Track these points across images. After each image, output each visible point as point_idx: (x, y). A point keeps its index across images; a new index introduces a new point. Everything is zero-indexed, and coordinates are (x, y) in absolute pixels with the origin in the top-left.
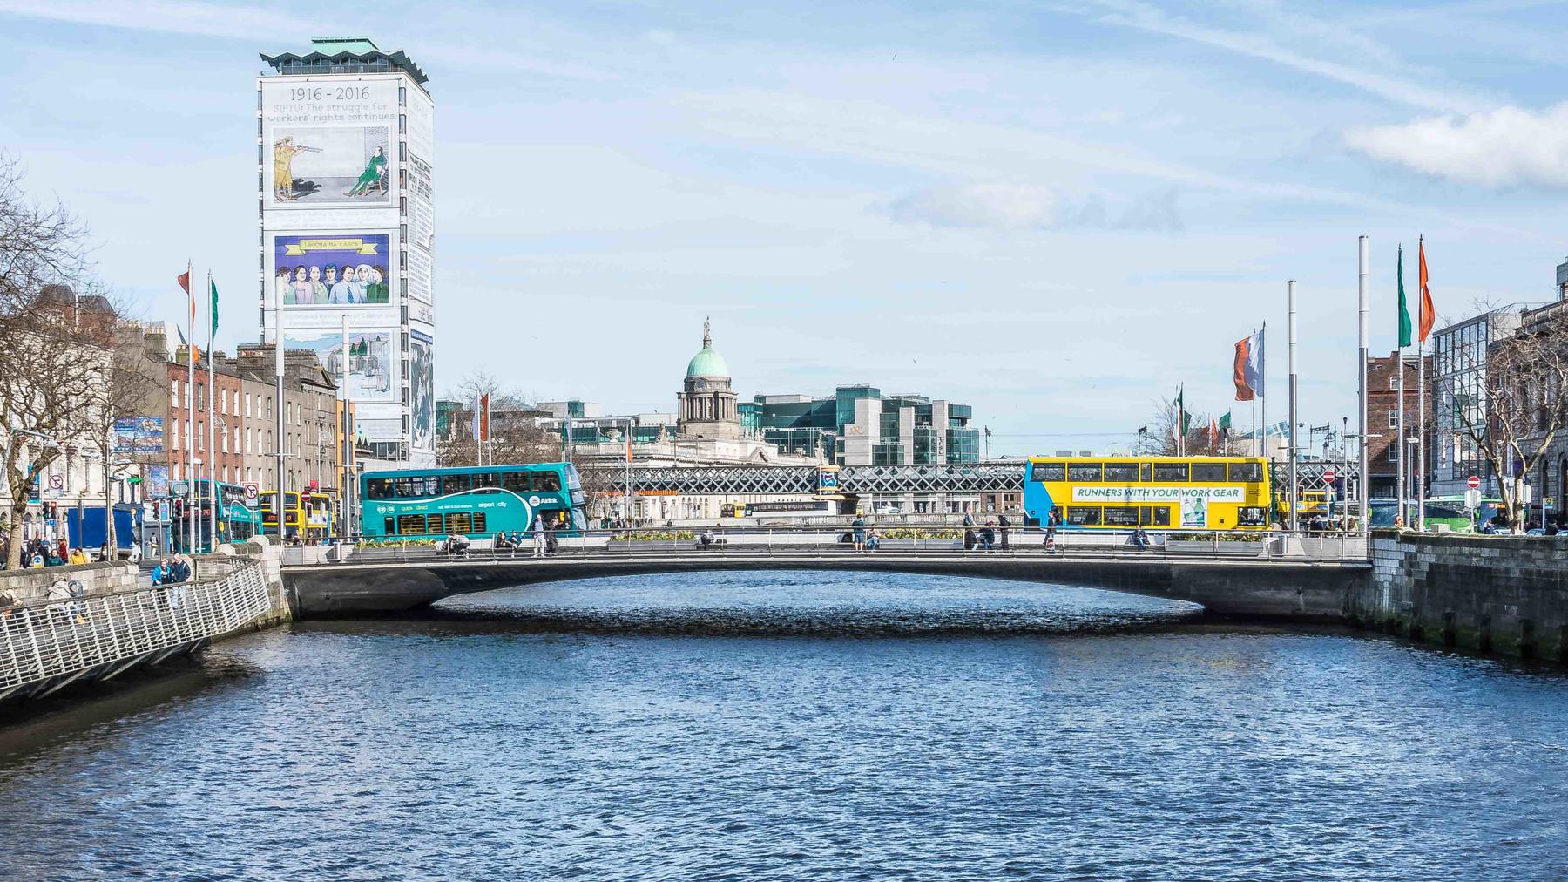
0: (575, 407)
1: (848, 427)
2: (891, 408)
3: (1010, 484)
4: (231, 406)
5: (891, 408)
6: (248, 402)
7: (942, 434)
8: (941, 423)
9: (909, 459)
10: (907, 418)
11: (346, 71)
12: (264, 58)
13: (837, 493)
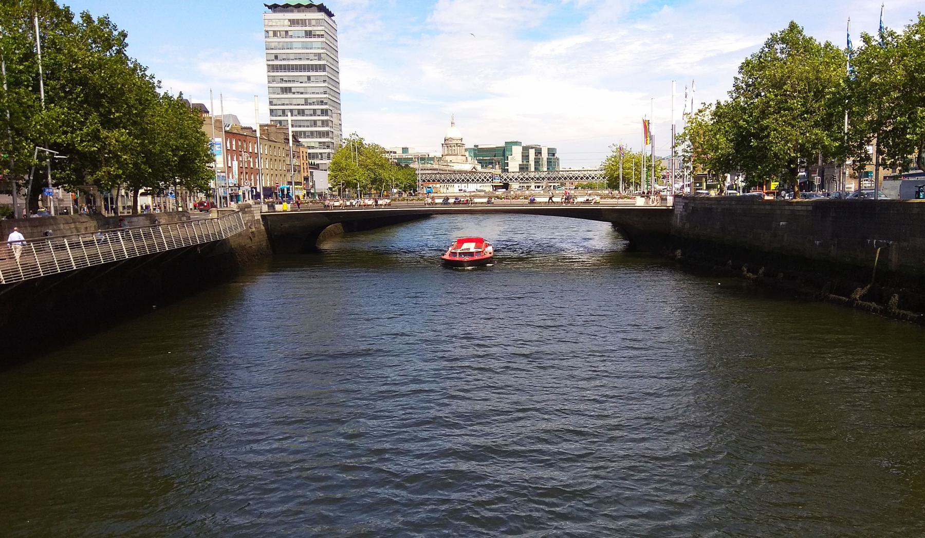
0: (405, 150)
1: (509, 157)
2: (526, 149)
3: (571, 178)
4: (253, 149)
5: (526, 149)
6: (234, 143)
7: (545, 159)
8: (545, 155)
9: (533, 169)
10: (532, 153)
11: (298, 12)
12: (266, 5)
13: (500, 182)
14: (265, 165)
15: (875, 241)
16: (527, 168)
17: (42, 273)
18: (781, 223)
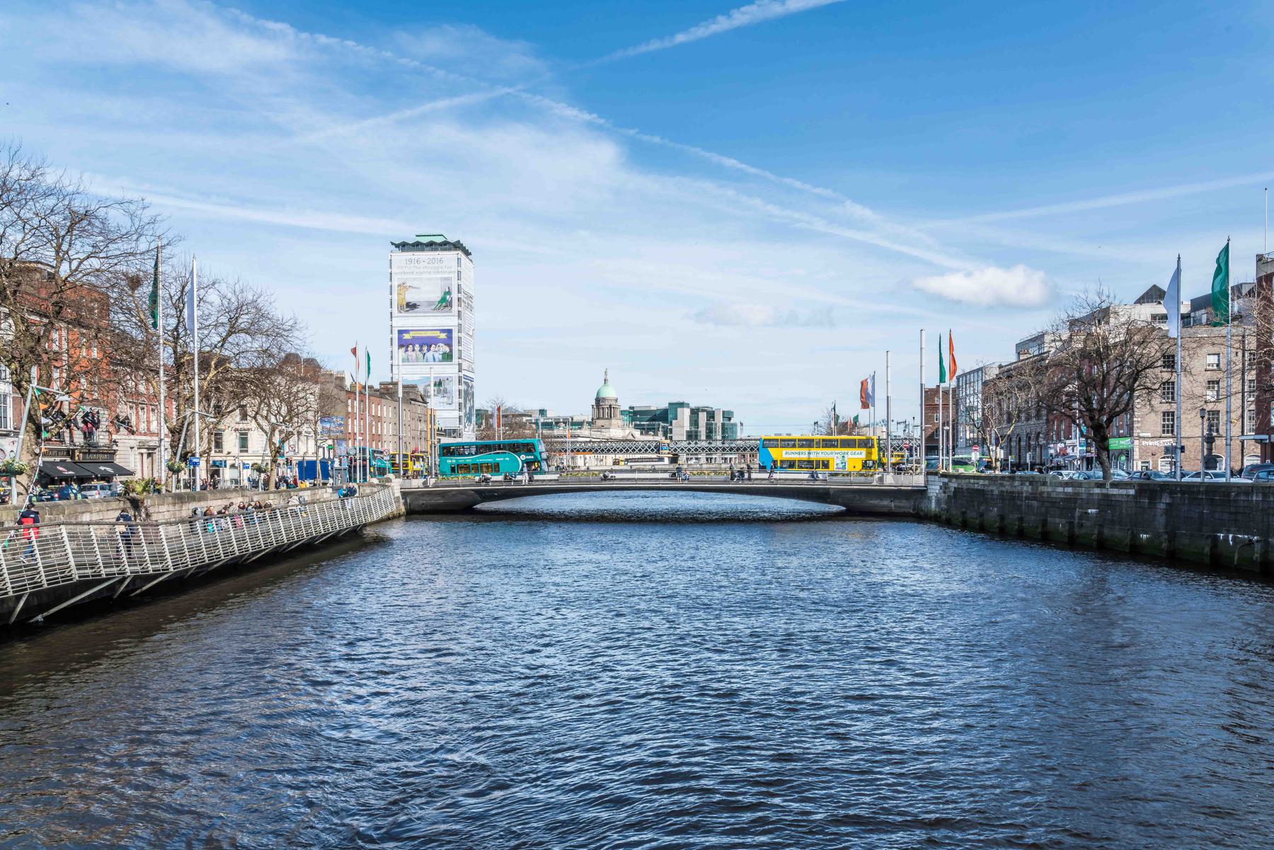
0: (542, 412)
1: (674, 421)
2: (695, 412)
4: (376, 412)
5: (695, 412)
7: (719, 425)
8: (719, 420)
9: (703, 437)
10: (703, 417)
12: (392, 244)
14: (388, 431)
15: (1231, 536)
16: (696, 436)
17: (206, 559)
18: (1090, 511)
